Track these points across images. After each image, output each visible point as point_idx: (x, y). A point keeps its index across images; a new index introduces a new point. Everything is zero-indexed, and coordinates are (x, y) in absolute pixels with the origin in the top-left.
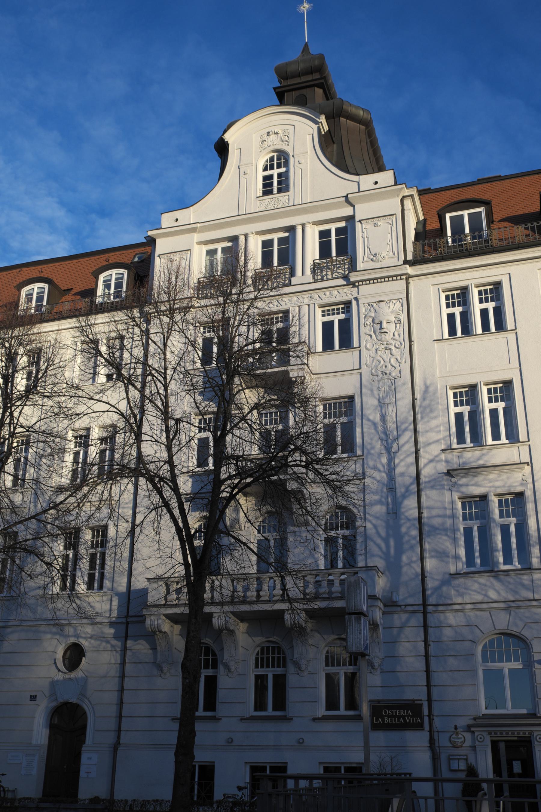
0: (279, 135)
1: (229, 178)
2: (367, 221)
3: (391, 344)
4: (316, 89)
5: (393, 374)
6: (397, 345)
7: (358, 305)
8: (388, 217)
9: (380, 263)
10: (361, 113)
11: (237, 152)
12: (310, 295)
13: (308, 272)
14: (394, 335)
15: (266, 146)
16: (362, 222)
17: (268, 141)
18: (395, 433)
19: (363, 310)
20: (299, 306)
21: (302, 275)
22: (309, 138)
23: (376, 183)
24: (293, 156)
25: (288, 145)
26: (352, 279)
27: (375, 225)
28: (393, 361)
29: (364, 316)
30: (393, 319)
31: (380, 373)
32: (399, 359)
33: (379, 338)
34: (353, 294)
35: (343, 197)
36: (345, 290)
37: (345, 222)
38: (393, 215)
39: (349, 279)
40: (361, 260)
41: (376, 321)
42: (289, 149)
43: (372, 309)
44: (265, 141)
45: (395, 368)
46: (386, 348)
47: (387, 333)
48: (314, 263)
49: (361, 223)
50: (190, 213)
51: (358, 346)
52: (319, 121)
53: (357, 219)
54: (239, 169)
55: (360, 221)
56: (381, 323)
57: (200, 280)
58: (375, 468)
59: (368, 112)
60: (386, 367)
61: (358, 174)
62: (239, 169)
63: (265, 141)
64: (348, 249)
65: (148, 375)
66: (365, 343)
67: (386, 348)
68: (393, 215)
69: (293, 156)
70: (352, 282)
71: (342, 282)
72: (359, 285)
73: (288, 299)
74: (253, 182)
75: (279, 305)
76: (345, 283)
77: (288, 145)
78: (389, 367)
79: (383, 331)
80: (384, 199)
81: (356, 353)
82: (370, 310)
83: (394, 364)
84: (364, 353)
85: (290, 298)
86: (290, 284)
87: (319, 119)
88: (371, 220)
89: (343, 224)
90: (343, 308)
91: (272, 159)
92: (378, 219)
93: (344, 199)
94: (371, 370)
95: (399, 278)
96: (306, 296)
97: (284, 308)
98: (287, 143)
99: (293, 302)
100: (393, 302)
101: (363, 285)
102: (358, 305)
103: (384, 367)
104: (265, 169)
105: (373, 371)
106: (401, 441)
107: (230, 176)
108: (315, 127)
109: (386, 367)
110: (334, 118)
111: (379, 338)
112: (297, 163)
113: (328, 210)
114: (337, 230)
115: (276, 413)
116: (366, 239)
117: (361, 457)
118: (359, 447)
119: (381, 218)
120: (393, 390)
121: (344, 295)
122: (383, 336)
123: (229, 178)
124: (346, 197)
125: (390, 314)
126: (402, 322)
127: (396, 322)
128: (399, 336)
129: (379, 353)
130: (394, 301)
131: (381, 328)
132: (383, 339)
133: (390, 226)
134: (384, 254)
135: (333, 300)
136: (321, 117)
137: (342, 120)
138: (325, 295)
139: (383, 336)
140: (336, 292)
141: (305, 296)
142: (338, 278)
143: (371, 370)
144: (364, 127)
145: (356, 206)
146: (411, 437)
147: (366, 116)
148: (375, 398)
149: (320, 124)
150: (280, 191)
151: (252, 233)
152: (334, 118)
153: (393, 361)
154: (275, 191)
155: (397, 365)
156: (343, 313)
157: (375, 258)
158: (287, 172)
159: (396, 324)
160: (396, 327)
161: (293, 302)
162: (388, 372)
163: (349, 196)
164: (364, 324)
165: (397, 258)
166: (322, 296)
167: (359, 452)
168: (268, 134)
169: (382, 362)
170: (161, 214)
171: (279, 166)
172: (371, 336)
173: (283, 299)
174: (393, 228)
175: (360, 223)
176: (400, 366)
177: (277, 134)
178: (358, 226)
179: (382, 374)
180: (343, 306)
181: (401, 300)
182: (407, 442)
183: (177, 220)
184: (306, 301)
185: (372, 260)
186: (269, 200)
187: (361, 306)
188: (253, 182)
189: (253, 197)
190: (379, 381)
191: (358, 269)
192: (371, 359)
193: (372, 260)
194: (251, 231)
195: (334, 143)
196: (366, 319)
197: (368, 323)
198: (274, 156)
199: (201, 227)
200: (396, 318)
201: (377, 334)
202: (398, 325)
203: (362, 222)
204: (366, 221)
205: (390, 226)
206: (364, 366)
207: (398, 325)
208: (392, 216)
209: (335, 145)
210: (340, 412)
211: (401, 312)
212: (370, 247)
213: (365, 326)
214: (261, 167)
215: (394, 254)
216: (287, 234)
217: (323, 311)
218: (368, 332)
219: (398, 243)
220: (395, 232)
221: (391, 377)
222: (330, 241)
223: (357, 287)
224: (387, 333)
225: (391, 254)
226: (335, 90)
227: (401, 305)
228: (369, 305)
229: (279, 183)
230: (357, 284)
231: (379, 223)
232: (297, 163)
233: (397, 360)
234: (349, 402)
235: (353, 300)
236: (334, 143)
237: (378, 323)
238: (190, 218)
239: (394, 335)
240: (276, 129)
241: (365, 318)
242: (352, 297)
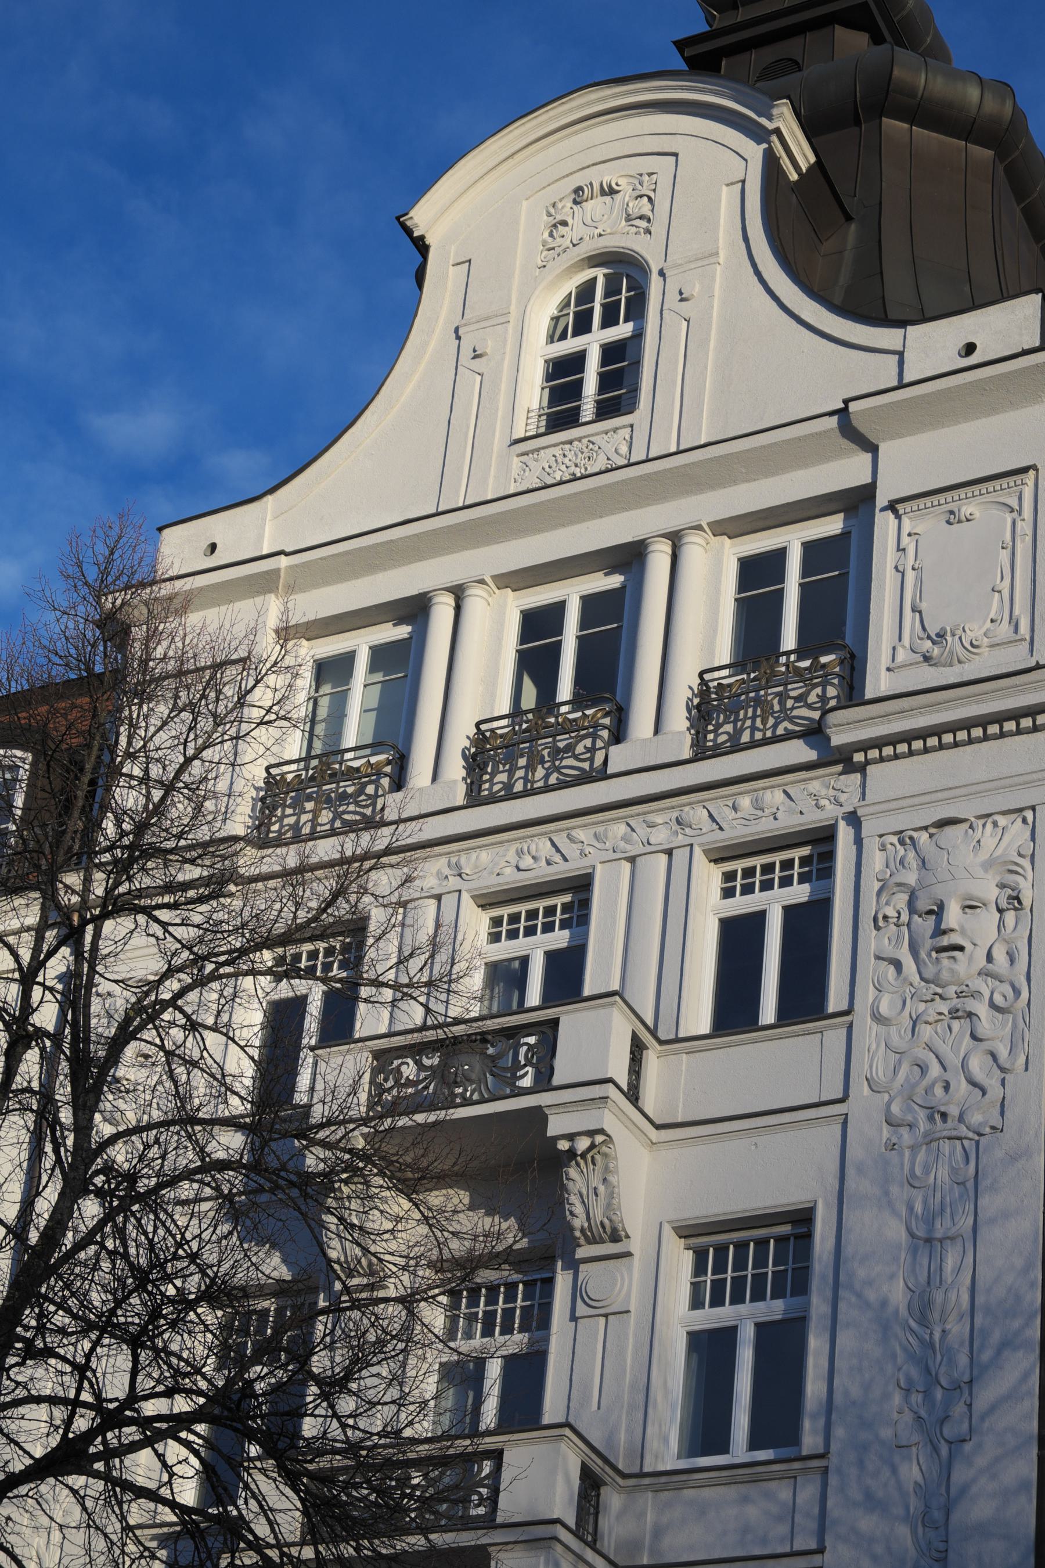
0: (618, 197)
1: (416, 378)
2: (921, 503)
3: (975, 995)
4: (840, 31)
5: (976, 1118)
6: (998, 999)
7: (859, 841)
8: (1004, 482)
9: (957, 668)
10: (973, 93)
11: (455, 276)
12: (675, 814)
13: (678, 720)
14: (989, 958)
15: (568, 243)
16: (899, 507)
17: (575, 222)
18: (963, 1360)
19: (876, 861)
20: (632, 860)
21: (656, 731)
22: (728, 198)
23: (970, 349)
24: (662, 273)
25: (648, 231)
26: (837, 739)
27: (953, 518)
28: (977, 1065)
29: (877, 885)
30: (991, 893)
31: (922, 1115)
32: (1003, 1052)
33: (930, 971)
34: (843, 798)
35: (831, 414)
36: (815, 786)
37: (841, 516)
38: (1025, 470)
39: (828, 739)
40: (885, 660)
41: (923, 905)
42: (652, 256)
43: (911, 854)
44: (564, 223)
45: (984, 1093)
46: (954, 1014)
47: (961, 948)
48: (703, 682)
49: (898, 517)
50: (264, 519)
51: (844, 1007)
52: (770, 126)
53: (882, 500)
54: (458, 338)
55: (892, 506)
56: (938, 912)
57: (273, 771)
58: (872, 1502)
59: (1005, 89)
60: (947, 1087)
61: (902, 323)
62: (458, 338)
63: (564, 223)
64: (844, 624)
65: (97, 1243)
66: (872, 992)
67: (954, 1014)
68: (1025, 470)
69: (662, 273)
70: (839, 748)
71: (799, 752)
72: (868, 762)
73: (591, 831)
74: (504, 386)
75: (557, 858)
76: (812, 755)
77: (648, 231)
78: (961, 1087)
79: (945, 941)
80: (993, 410)
81: (834, 1037)
82: (902, 862)
83: (979, 1075)
84: (867, 1032)
85: (600, 829)
86: (602, 775)
87: (770, 118)
88: (935, 499)
89: (832, 526)
90: (804, 861)
91: (586, 292)
92: (962, 492)
93: (834, 421)
94: (888, 1105)
95: (1026, 722)
96: (662, 816)
97: (574, 867)
98: (644, 224)
99: (608, 845)
100: (995, 824)
101: (882, 759)
102: (859, 841)
103: (939, 1091)
104: (558, 334)
105: (895, 1109)
106: (985, 1396)
107: (423, 365)
108: (755, 152)
109: (947, 1087)
110: (857, 123)
111: (930, 971)
112: (672, 296)
113: (774, 474)
114: (809, 547)
115: (512, 1287)
116: (910, 576)
117: (815, 1463)
118: (814, 1417)
119: (969, 490)
120: (970, 1184)
121: (806, 804)
122: (945, 962)
123: (416, 378)
124: (842, 413)
125: (980, 872)
126: (1027, 902)
127: (1003, 904)
128: (1012, 959)
129: (926, 1032)
130: (1002, 821)
131: (939, 931)
132: (945, 975)
133: (1009, 518)
134: (975, 631)
135: (765, 827)
136: (775, 112)
137: (890, 124)
138: (735, 808)
139: (945, 962)
140: (778, 796)
141: (659, 819)
142: (789, 736)
143: (888, 1105)
144: (989, 153)
145: (883, 448)
146: (1026, 1376)
147: (991, 105)
148: (895, 1213)
149: (774, 138)
150: (607, 410)
151: (482, 582)
152: (857, 123)
153: (977, 1065)
154: (588, 410)
155: (992, 1083)
156: (803, 879)
157: (936, 651)
158: (638, 335)
159: (1000, 911)
160: (1001, 921)
161: (608, 845)
162: (954, 1111)
163: (853, 407)
164: (875, 919)
165: (1026, 645)
166: (724, 814)
167: (810, 1440)
168: (578, 196)
169: (935, 1070)
170: (160, 529)
171: (610, 319)
172: (898, 965)
173: (574, 833)
174: (1019, 524)
175: (890, 515)
176: (1003, 1083)
177: (612, 192)
178: (885, 525)
179: (931, 1118)
180: (806, 851)
181: (1029, 815)
182: (1011, 1397)
183: (213, 547)
184: (661, 837)
185: (927, 659)
186: (557, 451)
187: (871, 844)
188: (504, 386)
189: (499, 440)
190: (914, 1148)
191: (869, 695)
192: (893, 1057)
193: (927, 659)
194: (475, 574)
195: (849, 218)
196: (884, 899)
197: (891, 912)
198: (592, 282)
199: (291, 568)
200: (1002, 886)
201: (923, 955)
202: (1010, 917)
203: (899, 507)
204: (914, 504)
205: (1009, 518)
206: (860, 1090)
207: (1010, 917)
208: (1018, 478)
209: (853, 227)
210: (759, 1280)
211: (1026, 863)
212: (924, 606)
213: (877, 928)
214: (540, 323)
215: (1016, 630)
216: (615, 581)
217: (729, 876)
218: (889, 951)
219: (1034, 581)
220: (1029, 539)
221: (963, 1131)
222: (778, 597)
223: (862, 769)
224: (961, 948)
225: (1004, 630)
226: (937, 36)
227: (1028, 834)
228: (902, 842)
229: (606, 382)
230: (859, 757)
231: (966, 510)
232: (672, 296)
233: (994, 1056)
234: (797, 1237)
235: (842, 825)
236: (849, 218)
237: (930, 912)
238: (260, 538)
239: (989, 958)
240: (608, 175)
241: (879, 893)
242: (840, 812)
